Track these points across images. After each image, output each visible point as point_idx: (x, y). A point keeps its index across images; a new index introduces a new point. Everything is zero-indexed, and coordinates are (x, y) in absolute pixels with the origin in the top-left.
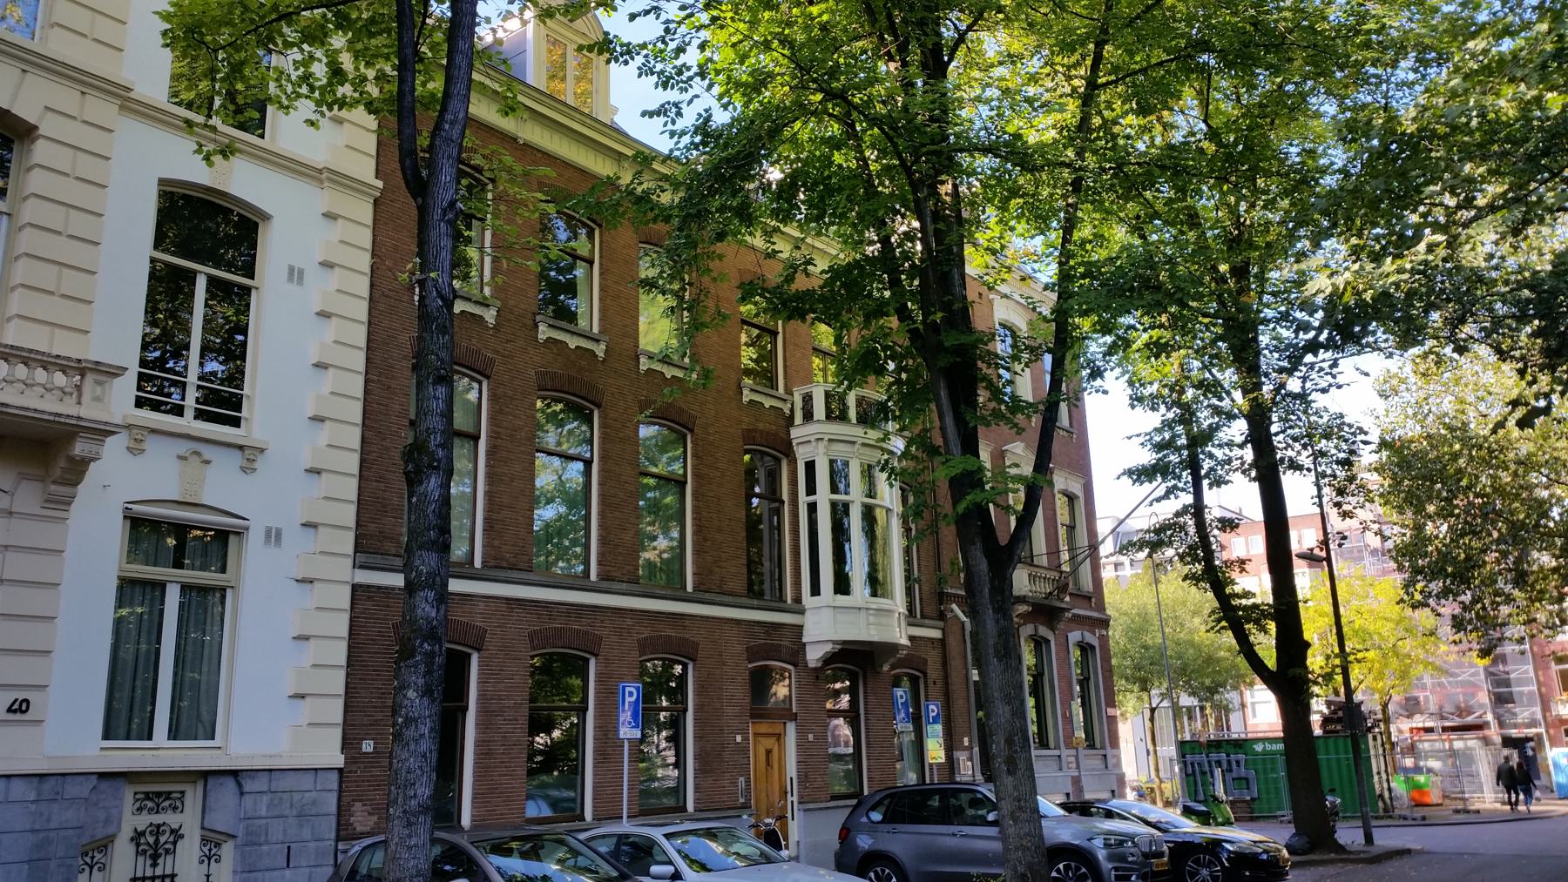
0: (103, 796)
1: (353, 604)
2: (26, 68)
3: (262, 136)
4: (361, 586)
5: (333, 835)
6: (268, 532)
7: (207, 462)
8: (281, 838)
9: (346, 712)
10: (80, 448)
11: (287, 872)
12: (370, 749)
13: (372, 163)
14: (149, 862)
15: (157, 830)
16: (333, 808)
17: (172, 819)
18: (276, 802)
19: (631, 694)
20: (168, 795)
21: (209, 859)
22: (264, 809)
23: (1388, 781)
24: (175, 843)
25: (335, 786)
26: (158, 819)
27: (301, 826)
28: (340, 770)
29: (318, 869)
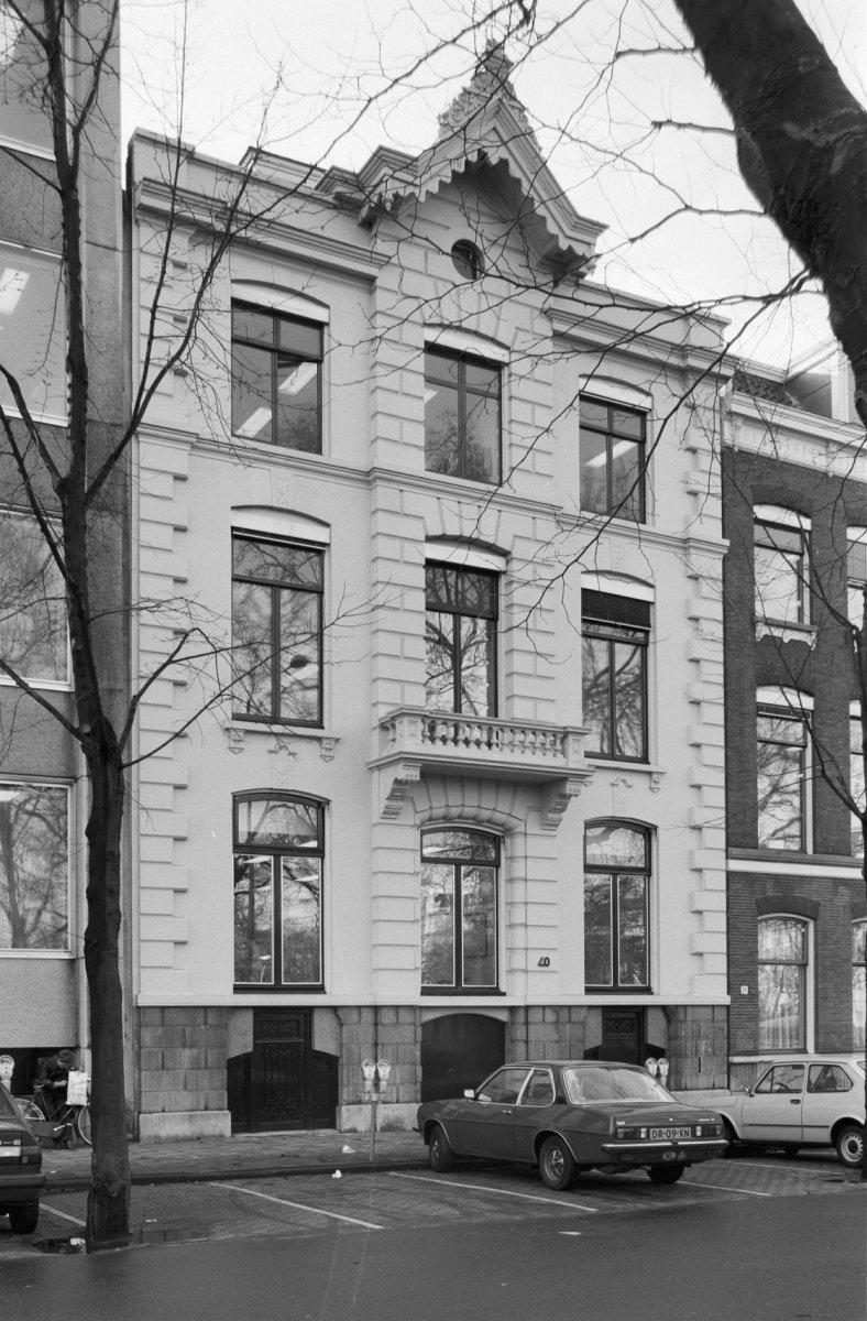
1: (728, 885)
2: (402, 488)
3: (319, 451)
7: (630, 786)
9: (728, 965)
10: (569, 788)
13: (719, 525)
23: (575, 995)
28: (728, 1007)
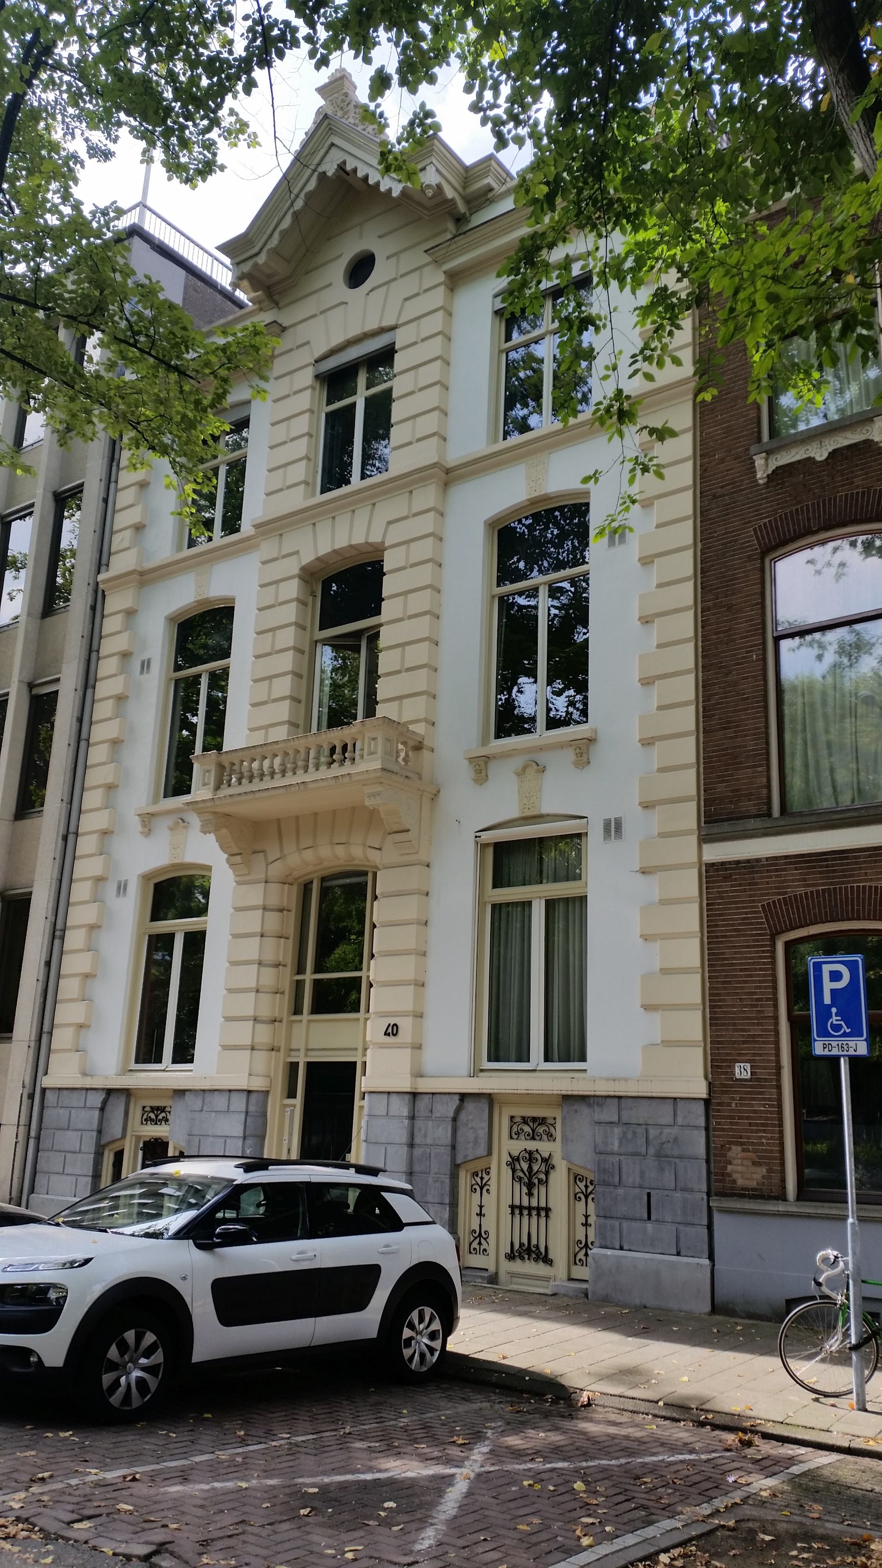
0: (471, 1117)
4: (713, 864)
5: (704, 1188)
6: (607, 825)
8: (638, 1181)
11: (649, 1226)
12: (746, 1075)
14: (525, 1190)
15: (531, 1156)
16: (702, 1151)
17: (544, 1147)
18: (630, 1135)
19: (836, 976)
20: (542, 1121)
21: (586, 1197)
22: (616, 1143)
24: (547, 1174)
25: (702, 1122)
26: (532, 1145)
27: (662, 1170)
29: (689, 1229)
